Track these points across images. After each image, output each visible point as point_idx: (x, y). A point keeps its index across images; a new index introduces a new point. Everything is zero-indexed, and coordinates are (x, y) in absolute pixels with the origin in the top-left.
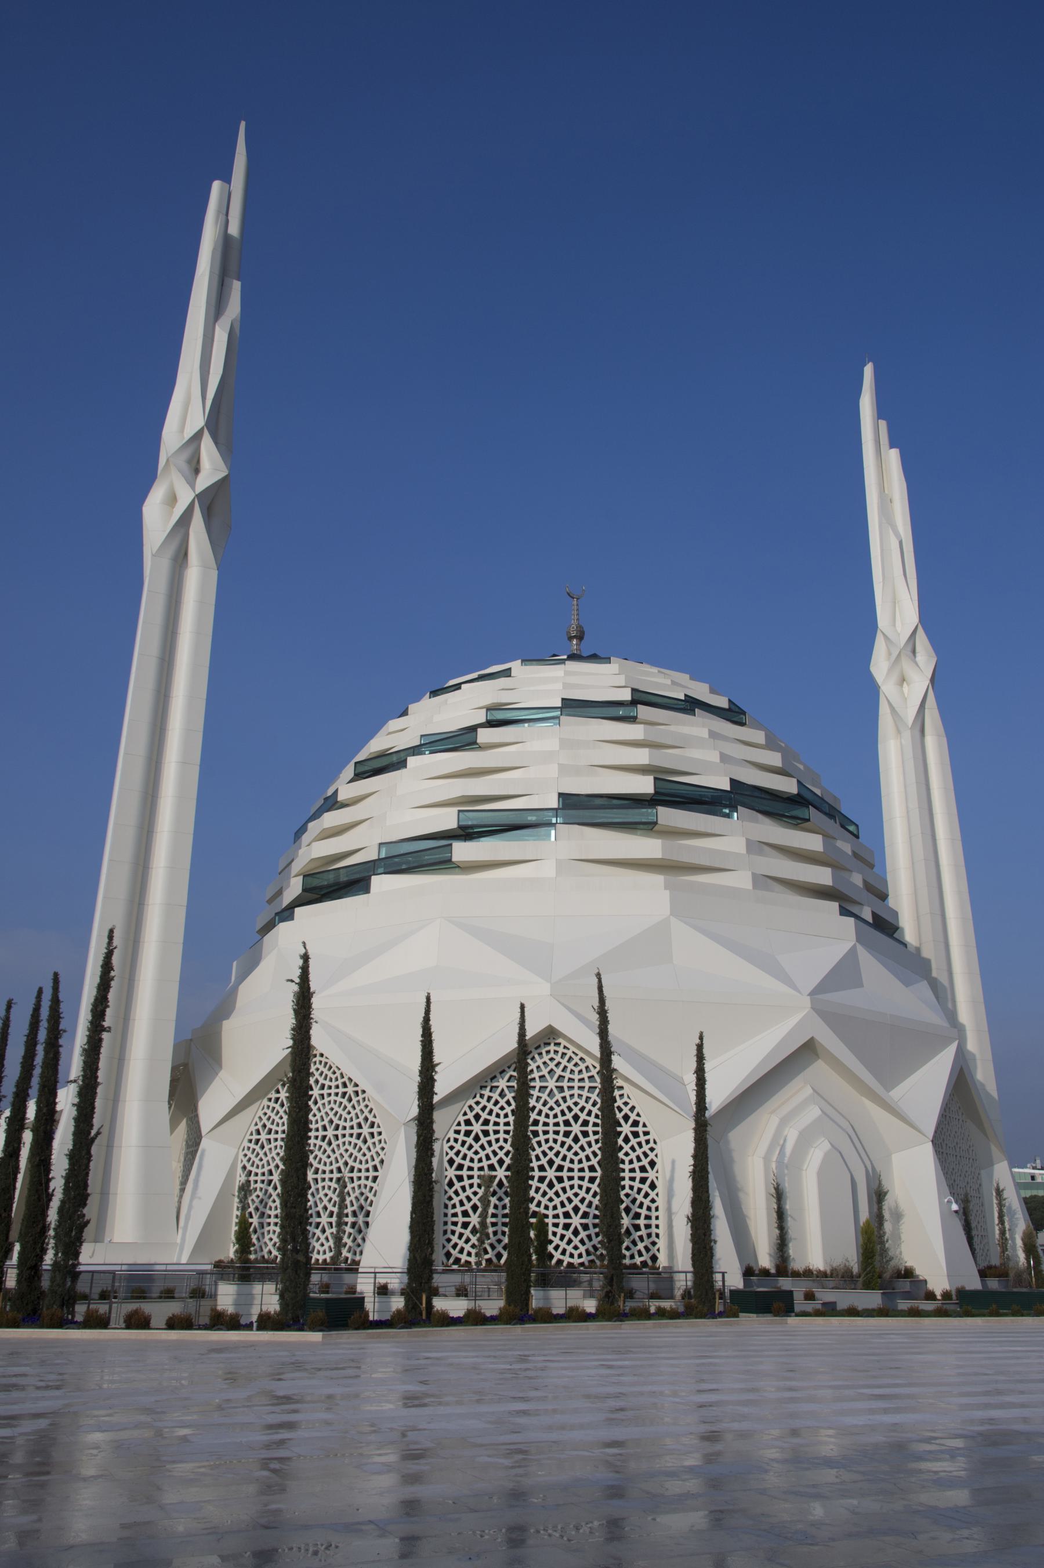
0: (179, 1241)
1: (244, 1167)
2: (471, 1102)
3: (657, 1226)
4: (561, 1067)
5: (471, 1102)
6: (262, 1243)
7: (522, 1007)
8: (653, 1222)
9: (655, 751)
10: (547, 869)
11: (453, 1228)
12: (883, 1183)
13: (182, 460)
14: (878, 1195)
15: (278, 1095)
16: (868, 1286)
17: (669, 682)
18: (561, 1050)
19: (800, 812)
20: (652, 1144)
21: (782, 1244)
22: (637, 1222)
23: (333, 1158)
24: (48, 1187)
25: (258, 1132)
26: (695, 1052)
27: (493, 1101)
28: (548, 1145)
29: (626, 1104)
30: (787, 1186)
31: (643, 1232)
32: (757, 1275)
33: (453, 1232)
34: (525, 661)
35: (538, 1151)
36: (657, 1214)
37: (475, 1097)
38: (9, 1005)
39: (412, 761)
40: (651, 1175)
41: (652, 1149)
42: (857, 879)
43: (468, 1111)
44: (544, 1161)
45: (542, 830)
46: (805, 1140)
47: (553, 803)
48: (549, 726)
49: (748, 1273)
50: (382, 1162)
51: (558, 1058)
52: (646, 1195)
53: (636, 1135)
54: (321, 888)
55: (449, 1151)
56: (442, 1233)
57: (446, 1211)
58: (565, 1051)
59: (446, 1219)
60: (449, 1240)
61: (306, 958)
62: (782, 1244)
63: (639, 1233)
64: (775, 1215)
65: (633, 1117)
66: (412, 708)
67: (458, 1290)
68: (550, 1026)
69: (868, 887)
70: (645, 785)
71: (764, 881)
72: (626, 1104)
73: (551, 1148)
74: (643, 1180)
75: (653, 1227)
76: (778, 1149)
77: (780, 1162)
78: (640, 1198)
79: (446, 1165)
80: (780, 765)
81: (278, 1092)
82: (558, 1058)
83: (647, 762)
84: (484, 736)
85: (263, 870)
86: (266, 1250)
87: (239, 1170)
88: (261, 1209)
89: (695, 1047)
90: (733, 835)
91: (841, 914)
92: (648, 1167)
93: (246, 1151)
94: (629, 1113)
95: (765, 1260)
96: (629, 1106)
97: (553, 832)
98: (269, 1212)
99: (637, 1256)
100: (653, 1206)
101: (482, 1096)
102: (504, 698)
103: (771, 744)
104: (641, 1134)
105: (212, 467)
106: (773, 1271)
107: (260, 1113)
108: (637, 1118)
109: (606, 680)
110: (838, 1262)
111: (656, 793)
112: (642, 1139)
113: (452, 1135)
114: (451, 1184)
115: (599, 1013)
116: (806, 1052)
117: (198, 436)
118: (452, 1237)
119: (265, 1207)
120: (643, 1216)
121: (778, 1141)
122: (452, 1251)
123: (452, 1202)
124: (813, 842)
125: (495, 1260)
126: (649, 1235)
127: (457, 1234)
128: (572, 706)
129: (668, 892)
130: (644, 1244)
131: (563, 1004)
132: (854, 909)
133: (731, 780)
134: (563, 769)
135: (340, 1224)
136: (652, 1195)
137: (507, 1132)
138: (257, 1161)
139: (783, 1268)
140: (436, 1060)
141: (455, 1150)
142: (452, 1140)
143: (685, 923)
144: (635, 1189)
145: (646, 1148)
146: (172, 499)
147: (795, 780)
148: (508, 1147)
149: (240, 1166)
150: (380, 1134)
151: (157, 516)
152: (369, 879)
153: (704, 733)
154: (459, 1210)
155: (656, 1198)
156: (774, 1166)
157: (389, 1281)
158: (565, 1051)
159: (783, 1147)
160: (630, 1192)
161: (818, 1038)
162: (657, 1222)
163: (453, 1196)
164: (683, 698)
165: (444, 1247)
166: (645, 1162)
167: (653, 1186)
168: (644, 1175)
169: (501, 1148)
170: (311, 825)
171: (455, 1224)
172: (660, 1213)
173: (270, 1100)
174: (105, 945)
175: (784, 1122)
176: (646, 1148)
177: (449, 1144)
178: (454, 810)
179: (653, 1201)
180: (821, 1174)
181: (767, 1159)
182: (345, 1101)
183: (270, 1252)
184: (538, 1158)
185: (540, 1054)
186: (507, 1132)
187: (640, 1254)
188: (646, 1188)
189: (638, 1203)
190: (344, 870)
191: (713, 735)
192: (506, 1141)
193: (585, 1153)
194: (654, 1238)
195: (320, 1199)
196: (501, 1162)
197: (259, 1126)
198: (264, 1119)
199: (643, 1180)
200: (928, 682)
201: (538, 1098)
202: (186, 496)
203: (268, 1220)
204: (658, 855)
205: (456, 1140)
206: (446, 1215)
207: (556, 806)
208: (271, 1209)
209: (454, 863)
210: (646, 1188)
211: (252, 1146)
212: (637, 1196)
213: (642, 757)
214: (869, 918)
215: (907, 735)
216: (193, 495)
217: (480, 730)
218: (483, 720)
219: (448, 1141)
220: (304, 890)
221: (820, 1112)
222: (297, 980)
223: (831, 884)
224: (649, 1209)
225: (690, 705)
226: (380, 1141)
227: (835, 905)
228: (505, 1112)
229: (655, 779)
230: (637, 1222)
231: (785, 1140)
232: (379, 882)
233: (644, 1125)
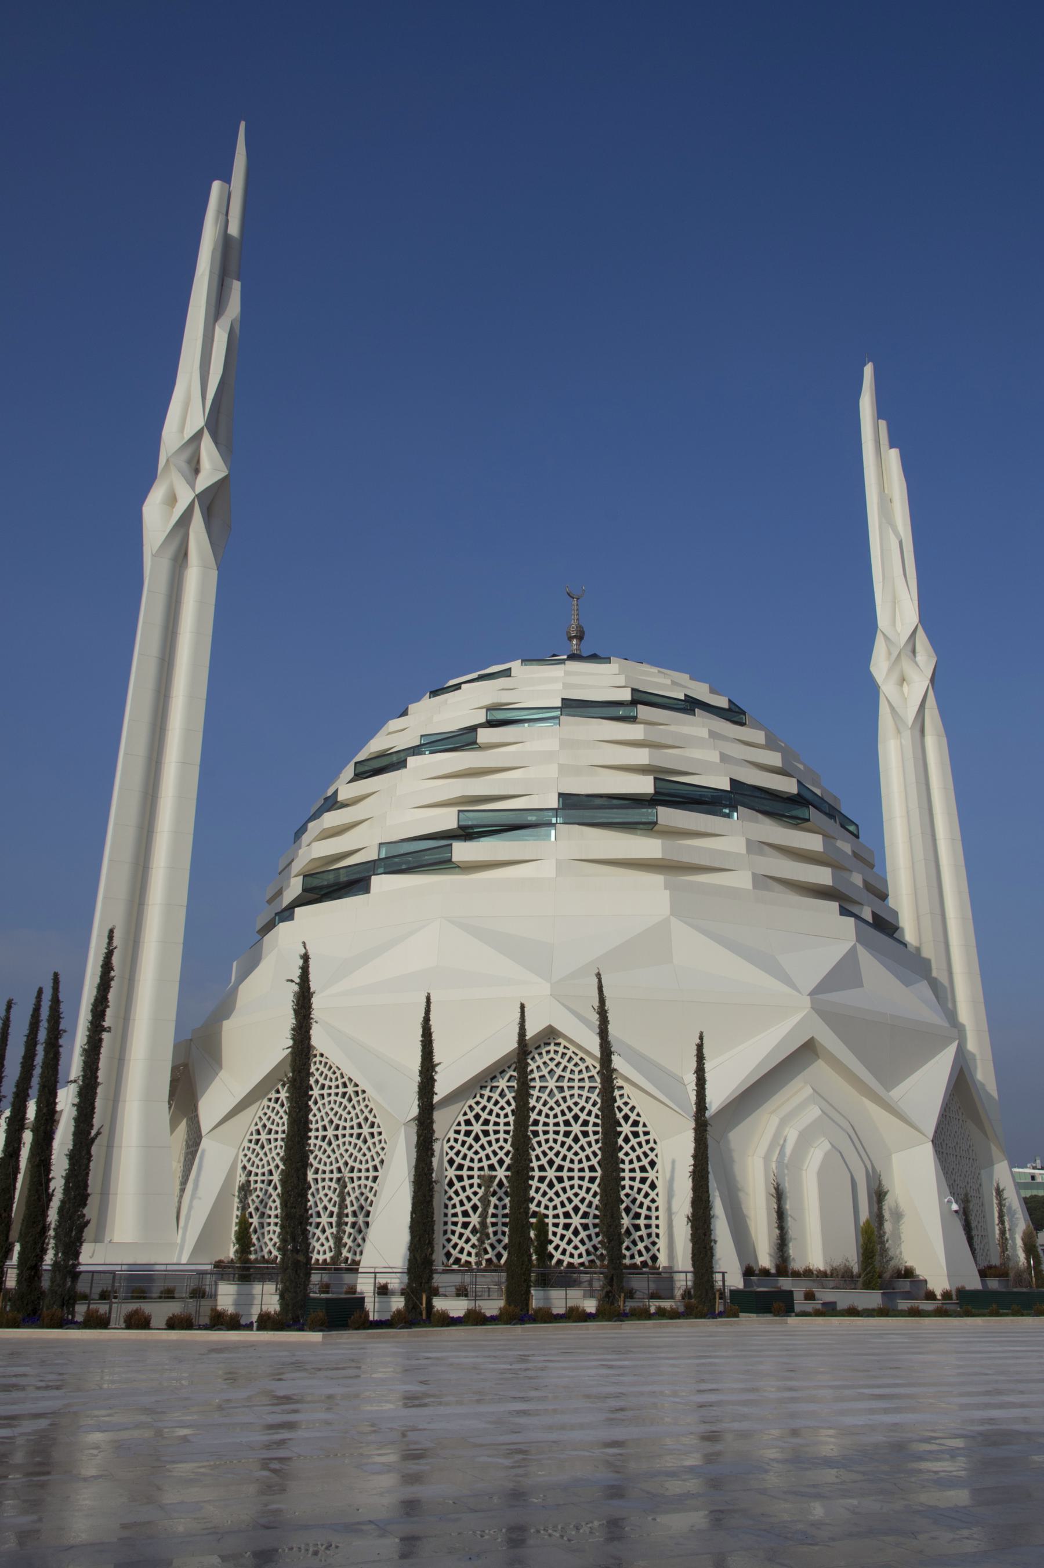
0: (179, 1241)
1: (244, 1167)
2: (472, 1102)
3: (657, 1226)
4: (561, 1067)
5: (472, 1102)
6: (262, 1243)
7: (522, 1007)
8: (654, 1222)
10: (545, 870)
11: (454, 1228)
12: (884, 1182)
14: (879, 1195)
15: (278, 1095)
16: (868, 1285)
17: (669, 682)
18: (561, 1050)
19: (800, 812)
20: (652, 1144)
21: (782, 1243)
22: (637, 1222)
23: (333, 1158)
24: (48, 1187)
25: (258, 1133)
26: (695, 1052)
27: (493, 1101)
28: (549, 1145)
29: (626, 1104)
30: (787, 1186)
31: (643, 1232)
32: (757, 1275)
33: (453, 1232)
34: (525, 661)
35: (538, 1151)
36: (657, 1214)
37: (475, 1097)
38: (9, 1006)
39: (411, 761)
40: (651, 1175)
41: (652, 1149)
43: (468, 1111)
44: (544, 1161)
45: (542, 830)
46: (805, 1140)
47: (553, 803)
48: (549, 725)
49: (748, 1273)
50: (382, 1162)
51: (558, 1058)
52: (647, 1195)
54: (321, 888)
55: (449, 1151)
56: (442, 1233)
58: (565, 1051)
59: (446, 1219)
60: (449, 1240)
61: (306, 958)
62: (782, 1243)
63: (639, 1233)
64: (775, 1215)
65: (633, 1117)
66: (412, 708)
68: (550, 1026)
70: (645, 785)
71: (764, 881)
72: (626, 1104)
74: (643, 1180)
75: (654, 1227)
76: (779, 1148)
77: (780, 1161)
78: (640, 1198)
79: (446, 1165)
80: (780, 765)
81: (278, 1092)
82: (558, 1058)
83: (647, 762)
84: (484, 736)
85: (263, 870)
86: (266, 1251)
87: (240, 1170)
88: (261, 1209)
89: (695, 1047)
90: (733, 835)
91: (841, 914)
92: (648, 1167)
93: (246, 1151)
94: (629, 1113)
95: (765, 1260)
96: (629, 1106)
97: (553, 832)
98: (269, 1212)
99: (637, 1256)
100: (653, 1206)
101: (482, 1096)
102: (505, 698)
103: (771, 744)
104: (641, 1134)
106: (773, 1271)
107: (260, 1113)
108: (638, 1118)
109: (605, 680)
110: (838, 1262)
111: (656, 793)
112: (642, 1138)
113: (452, 1135)
114: (451, 1184)
115: (599, 1013)
116: (806, 1052)
118: (452, 1237)
119: (265, 1207)
120: (643, 1216)
121: (778, 1141)
122: (452, 1251)
123: (452, 1202)
124: (813, 842)
125: (495, 1260)
126: (649, 1235)
127: (457, 1234)
128: (572, 706)
129: (668, 892)
130: (644, 1244)
131: (563, 1004)
133: (731, 779)
135: (340, 1224)
136: (652, 1194)
137: (507, 1132)
138: (257, 1161)
139: (783, 1268)
141: (455, 1150)
142: (452, 1140)
143: (685, 923)
145: (646, 1148)
147: (795, 780)
148: (508, 1147)
149: (240, 1166)
150: (380, 1134)
152: (369, 879)
153: (704, 733)
154: (459, 1210)
155: (656, 1198)
156: (774, 1165)
158: (565, 1051)
159: (783, 1147)
160: (630, 1192)
161: (818, 1038)
162: (657, 1222)
163: (454, 1196)
164: (683, 698)
166: (645, 1162)
167: (653, 1186)
168: (644, 1175)
169: (501, 1148)
170: (311, 825)
171: (455, 1224)
172: (660, 1213)
173: (270, 1100)
174: (105, 945)
175: (783, 1123)
176: (646, 1148)
177: (449, 1144)
178: (454, 810)
179: (653, 1201)
180: (822, 1173)
181: (767, 1159)
182: (345, 1101)
183: (270, 1252)
184: (538, 1158)
185: (540, 1054)
186: (507, 1132)
187: (640, 1254)
188: (646, 1188)
189: (638, 1203)
191: (713, 734)
192: (506, 1141)
194: (654, 1238)
195: (320, 1199)
196: (501, 1162)
197: (260, 1126)
198: (265, 1119)
199: (643, 1180)
200: (927, 682)
201: (538, 1098)
203: (268, 1220)
204: (658, 855)
205: (456, 1140)
206: (446, 1215)
207: (556, 806)
208: (271, 1209)
209: (453, 863)
210: (646, 1188)
211: (252, 1146)
212: (637, 1196)
213: (642, 757)
217: (480, 730)
218: (483, 720)
219: (449, 1141)
220: (304, 890)
222: (298, 980)
224: (649, 1209)
225: (690, 705)
227: (835, 905)
229: (655, 779)
230: (637, 1222)
231: (785, 1141)
232: (379, 882)
233: (645, 1125)
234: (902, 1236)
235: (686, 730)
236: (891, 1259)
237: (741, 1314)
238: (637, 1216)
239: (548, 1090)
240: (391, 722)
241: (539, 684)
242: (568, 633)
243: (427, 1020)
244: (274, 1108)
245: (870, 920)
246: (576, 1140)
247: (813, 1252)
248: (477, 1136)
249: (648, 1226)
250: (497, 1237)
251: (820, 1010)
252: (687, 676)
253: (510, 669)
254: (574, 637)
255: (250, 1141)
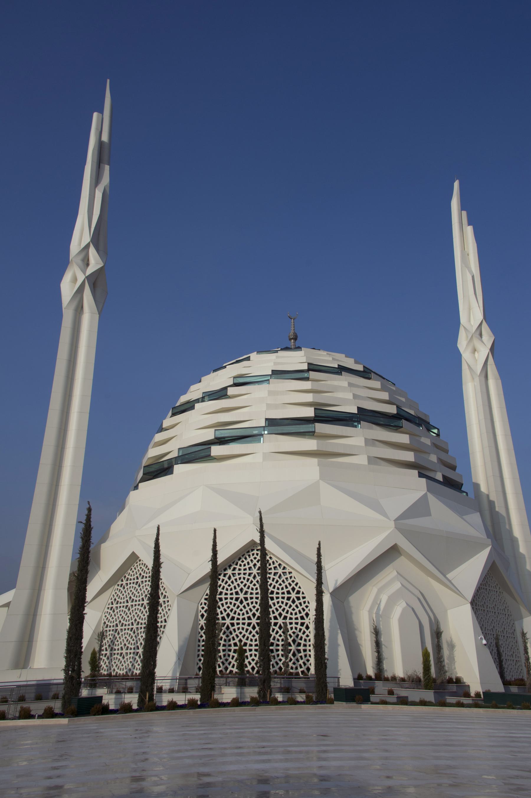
7: (215, 530)
9: (317, 395)
10: (257, 458)
13: (79, 260)
14: (437, 634)
15: (122, 583)
16: (427, 687)
17: (331, 359)
19: (397, 423)
20: (307, 604)
22: (299, 648)
26: (316, 552)
27: (275, 581)
28: (279, 605)
29: (293, 581)
30: (382, 628)
31: (302, 654)
32: (365, 680)
34: (259, 352)
35: (222, 609)
41: (307, 607)
42: (433, 458)
44: (277, 614)
46: (392, 601)
48: (265, 384)
49: (358, 678)
52: (304, 632)
53: (298, 598)
55: (201, 610)
56: (196, 656)
57: (199, 643)
63: (300, 655)
64: (374, 644)
65: (297, 588)
66: (203, 379)
67: (197, 689)
68: (253, 540)
69: (442, 462)
70: (310, 412)
71: (373, 460)
72: (293, 581)
73: (280, 607)
74: (302, 624)
75: (308, 651)
76: (377, 606)
77: (377, 614)
78: (301, 634)
79: (200, 617)
80: (388, 399)
81: (122, 581)
84: (231, 391)
85: (124, 462)
86: (112, 669)
88: (112, 646)
89: (316, 550)
90: (357, 437)
91: (419, 477)
94: (295, 587)
95: (371, 671)
96: (295, 583)
99: (299, 668)
100: (308, 639)
102: (244, 371)
103: (383, 389)
104: (301, 598)
105: (95, 262)
106: (373, 677)
107: (114, 593)
108: (299, 589)
109: (296, 360)
111: (316, 416)
112: (302, 601)
115: (260, 532)
116: (391, 553)
117: (87, 247)
119: (113, 645)
120: (302, 645)
121: (376, 602)
124: (404, 439)
125: (224, 670)
126: (306, 656)
130: (303, 661)
132: (431, 474)
133: (358, 408)
134: (269, 406)
137: (257, 598)
139: (380, 675)
140: (161, 560)
142: (203, 604)
143: (328, 484)
144: (298, 629)
145: (304, 606)
146: (75, 280)
147: (395, 406)
148: (257, 606)
149: (103, 622)
150: (168, 601)
151: (67, 288)
153: (345, 384)
155: (309, 634)
156: (374, 616)
157: (163, 684)
159: (379, 604)
164: (337, 367)
165: (198, 664)
166: (303, 614)
168: (303, 621)
169: (254, 607)
173: (118, 585)
175: (380, 591)
176: (304, 606)
177: (202, 606)
178: (213, 430)
181: (370, 612)
183: (114, 670)
184: (273, 612)
185: (249, 556)
186: (257, 598)
190: (167, 462)
191: (350, 385)
192: (256, 603)
193: (299, 609)
194: (308, 657)
196: (254, 615)
197: (113, 600)
198: (115, 595)
199: (302, 624)
200: (488, 351)
201: (223, 580)
202: (81, 278)
204: (315, 448)
206: (199, 646)
207: (264, 425)
209: (212, 457)
210: (304, 628)
211: (109, 611)
212: (299, 633)
213: (309, 398)
214: (441, 479)
215: (477, 379)
216: (84, 277)
217: (228, 388)
218: (232, 383)
219: (201, 604)
220: (144, 474)
221: (400, 585)
222: (84, 522)
223: (414, 461)
225: (341, 370)
226: (168, 605)
228: (282, 586)
229: (315, 409)
230: (299, 648)
231: (380, 602)
232: (178, 468)
233: (303, 593)
234: (456, 658)
235: (336, 383)
236: (446, 672)
237: (335, 702)
238: (299, 644)
239: (253, 575)
240: (192, 387)
241: (261, 363)
242: (289, 336)
243: (157, 539)
244: (133, 587)
245: (441, 479)
246: (294, 602)
247: (398, 666)
248: (242, 600)
249: (305, 651)
250: (225, 658)
251: (398, 528)
252: (344, 355)
253: (249, 357)
254: (292, 339)
255: (108, 608)
